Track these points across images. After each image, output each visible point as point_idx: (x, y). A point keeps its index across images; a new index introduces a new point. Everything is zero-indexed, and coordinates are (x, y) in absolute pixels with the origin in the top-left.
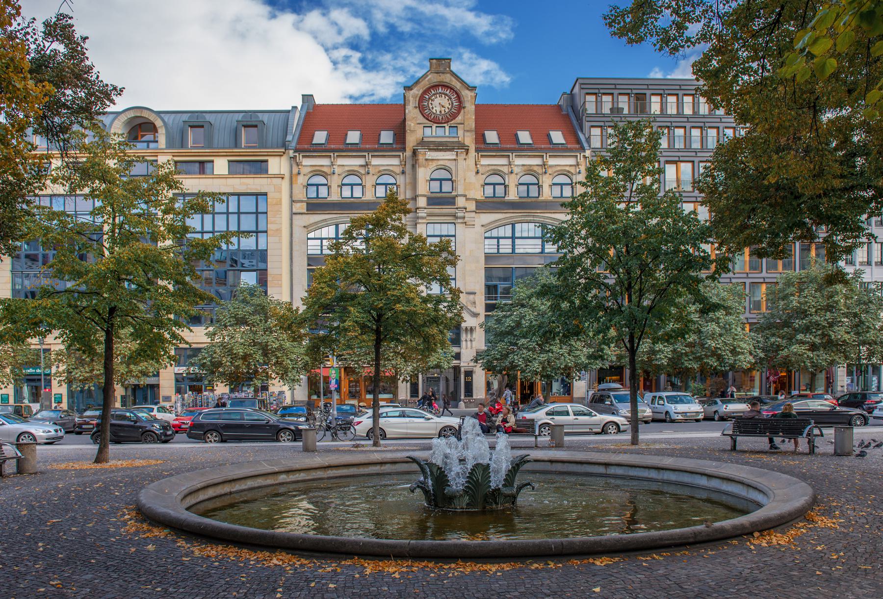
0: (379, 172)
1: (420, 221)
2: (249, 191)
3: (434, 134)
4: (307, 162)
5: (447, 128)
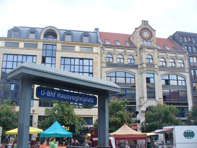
0: (129, 54)
2: (30, 54)
4: (106, 49)
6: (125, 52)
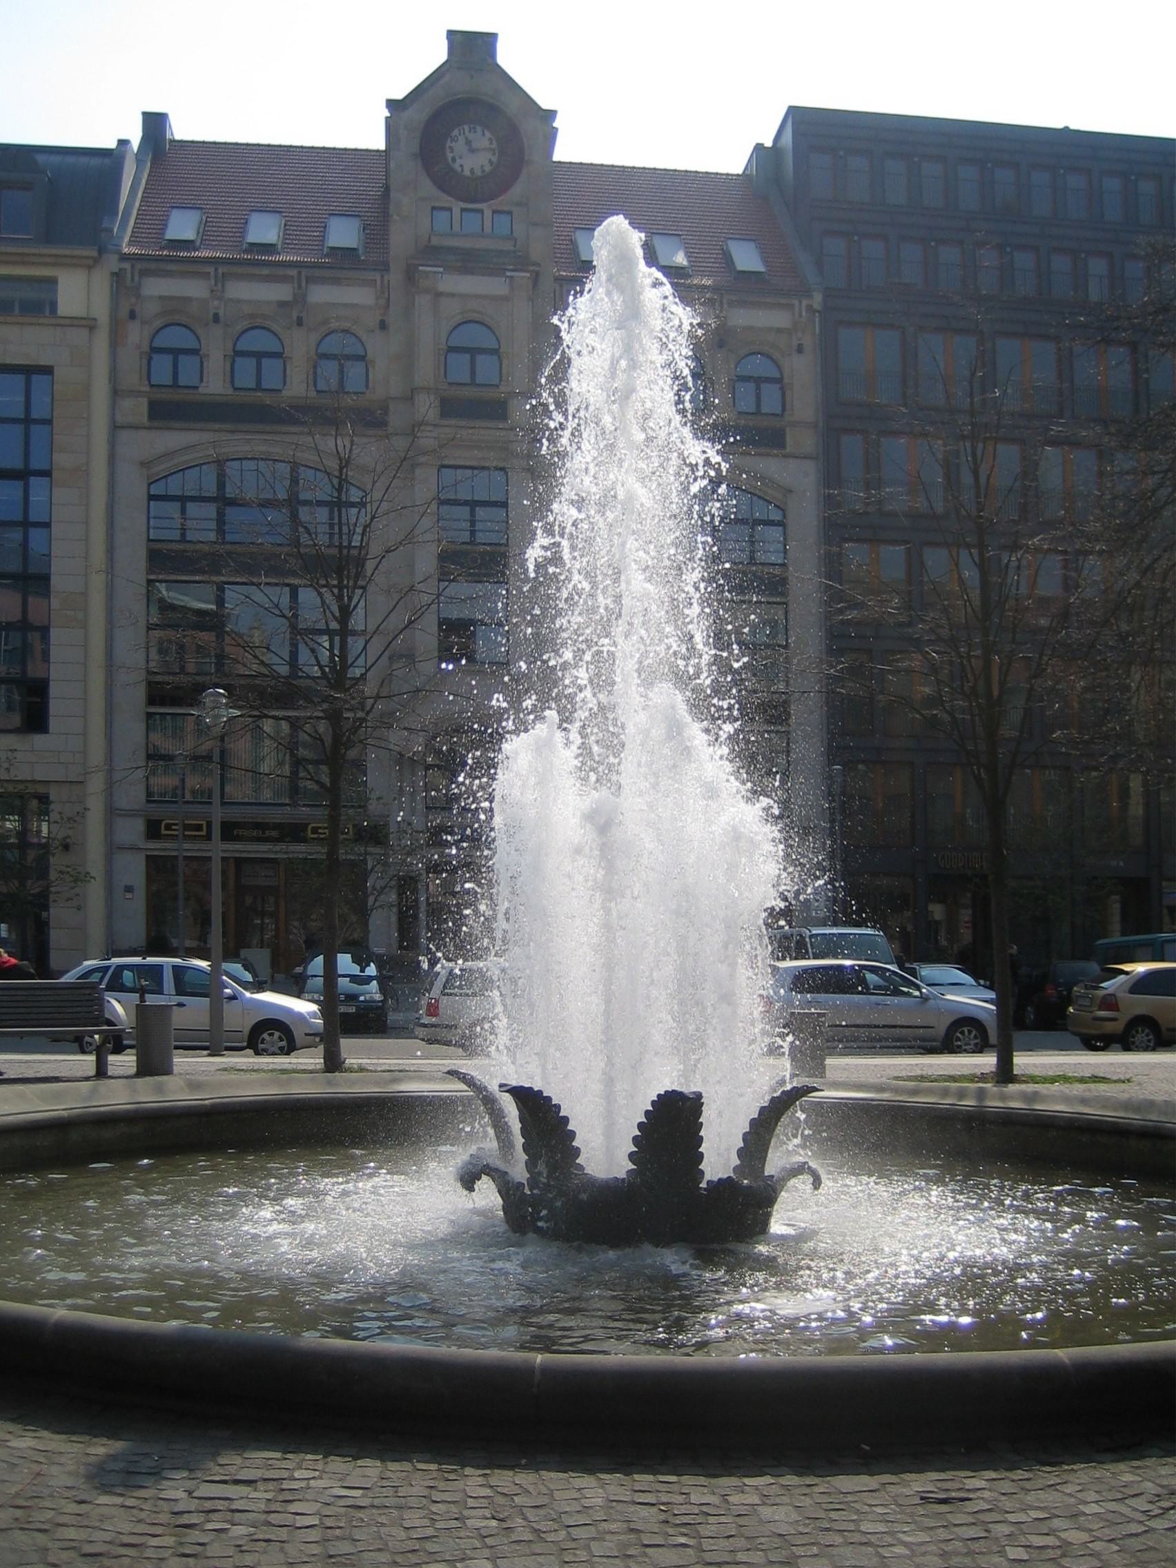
1: (422, 459)
3: (456, 227)
5: (488, 213)
6: (300, 299)
